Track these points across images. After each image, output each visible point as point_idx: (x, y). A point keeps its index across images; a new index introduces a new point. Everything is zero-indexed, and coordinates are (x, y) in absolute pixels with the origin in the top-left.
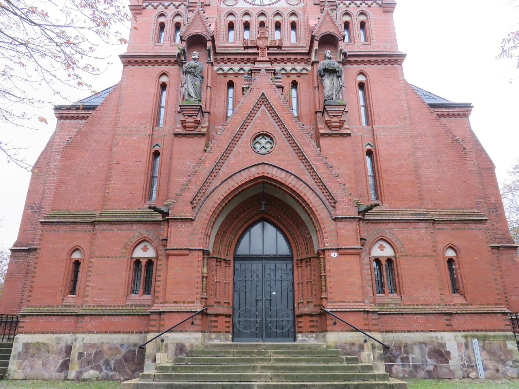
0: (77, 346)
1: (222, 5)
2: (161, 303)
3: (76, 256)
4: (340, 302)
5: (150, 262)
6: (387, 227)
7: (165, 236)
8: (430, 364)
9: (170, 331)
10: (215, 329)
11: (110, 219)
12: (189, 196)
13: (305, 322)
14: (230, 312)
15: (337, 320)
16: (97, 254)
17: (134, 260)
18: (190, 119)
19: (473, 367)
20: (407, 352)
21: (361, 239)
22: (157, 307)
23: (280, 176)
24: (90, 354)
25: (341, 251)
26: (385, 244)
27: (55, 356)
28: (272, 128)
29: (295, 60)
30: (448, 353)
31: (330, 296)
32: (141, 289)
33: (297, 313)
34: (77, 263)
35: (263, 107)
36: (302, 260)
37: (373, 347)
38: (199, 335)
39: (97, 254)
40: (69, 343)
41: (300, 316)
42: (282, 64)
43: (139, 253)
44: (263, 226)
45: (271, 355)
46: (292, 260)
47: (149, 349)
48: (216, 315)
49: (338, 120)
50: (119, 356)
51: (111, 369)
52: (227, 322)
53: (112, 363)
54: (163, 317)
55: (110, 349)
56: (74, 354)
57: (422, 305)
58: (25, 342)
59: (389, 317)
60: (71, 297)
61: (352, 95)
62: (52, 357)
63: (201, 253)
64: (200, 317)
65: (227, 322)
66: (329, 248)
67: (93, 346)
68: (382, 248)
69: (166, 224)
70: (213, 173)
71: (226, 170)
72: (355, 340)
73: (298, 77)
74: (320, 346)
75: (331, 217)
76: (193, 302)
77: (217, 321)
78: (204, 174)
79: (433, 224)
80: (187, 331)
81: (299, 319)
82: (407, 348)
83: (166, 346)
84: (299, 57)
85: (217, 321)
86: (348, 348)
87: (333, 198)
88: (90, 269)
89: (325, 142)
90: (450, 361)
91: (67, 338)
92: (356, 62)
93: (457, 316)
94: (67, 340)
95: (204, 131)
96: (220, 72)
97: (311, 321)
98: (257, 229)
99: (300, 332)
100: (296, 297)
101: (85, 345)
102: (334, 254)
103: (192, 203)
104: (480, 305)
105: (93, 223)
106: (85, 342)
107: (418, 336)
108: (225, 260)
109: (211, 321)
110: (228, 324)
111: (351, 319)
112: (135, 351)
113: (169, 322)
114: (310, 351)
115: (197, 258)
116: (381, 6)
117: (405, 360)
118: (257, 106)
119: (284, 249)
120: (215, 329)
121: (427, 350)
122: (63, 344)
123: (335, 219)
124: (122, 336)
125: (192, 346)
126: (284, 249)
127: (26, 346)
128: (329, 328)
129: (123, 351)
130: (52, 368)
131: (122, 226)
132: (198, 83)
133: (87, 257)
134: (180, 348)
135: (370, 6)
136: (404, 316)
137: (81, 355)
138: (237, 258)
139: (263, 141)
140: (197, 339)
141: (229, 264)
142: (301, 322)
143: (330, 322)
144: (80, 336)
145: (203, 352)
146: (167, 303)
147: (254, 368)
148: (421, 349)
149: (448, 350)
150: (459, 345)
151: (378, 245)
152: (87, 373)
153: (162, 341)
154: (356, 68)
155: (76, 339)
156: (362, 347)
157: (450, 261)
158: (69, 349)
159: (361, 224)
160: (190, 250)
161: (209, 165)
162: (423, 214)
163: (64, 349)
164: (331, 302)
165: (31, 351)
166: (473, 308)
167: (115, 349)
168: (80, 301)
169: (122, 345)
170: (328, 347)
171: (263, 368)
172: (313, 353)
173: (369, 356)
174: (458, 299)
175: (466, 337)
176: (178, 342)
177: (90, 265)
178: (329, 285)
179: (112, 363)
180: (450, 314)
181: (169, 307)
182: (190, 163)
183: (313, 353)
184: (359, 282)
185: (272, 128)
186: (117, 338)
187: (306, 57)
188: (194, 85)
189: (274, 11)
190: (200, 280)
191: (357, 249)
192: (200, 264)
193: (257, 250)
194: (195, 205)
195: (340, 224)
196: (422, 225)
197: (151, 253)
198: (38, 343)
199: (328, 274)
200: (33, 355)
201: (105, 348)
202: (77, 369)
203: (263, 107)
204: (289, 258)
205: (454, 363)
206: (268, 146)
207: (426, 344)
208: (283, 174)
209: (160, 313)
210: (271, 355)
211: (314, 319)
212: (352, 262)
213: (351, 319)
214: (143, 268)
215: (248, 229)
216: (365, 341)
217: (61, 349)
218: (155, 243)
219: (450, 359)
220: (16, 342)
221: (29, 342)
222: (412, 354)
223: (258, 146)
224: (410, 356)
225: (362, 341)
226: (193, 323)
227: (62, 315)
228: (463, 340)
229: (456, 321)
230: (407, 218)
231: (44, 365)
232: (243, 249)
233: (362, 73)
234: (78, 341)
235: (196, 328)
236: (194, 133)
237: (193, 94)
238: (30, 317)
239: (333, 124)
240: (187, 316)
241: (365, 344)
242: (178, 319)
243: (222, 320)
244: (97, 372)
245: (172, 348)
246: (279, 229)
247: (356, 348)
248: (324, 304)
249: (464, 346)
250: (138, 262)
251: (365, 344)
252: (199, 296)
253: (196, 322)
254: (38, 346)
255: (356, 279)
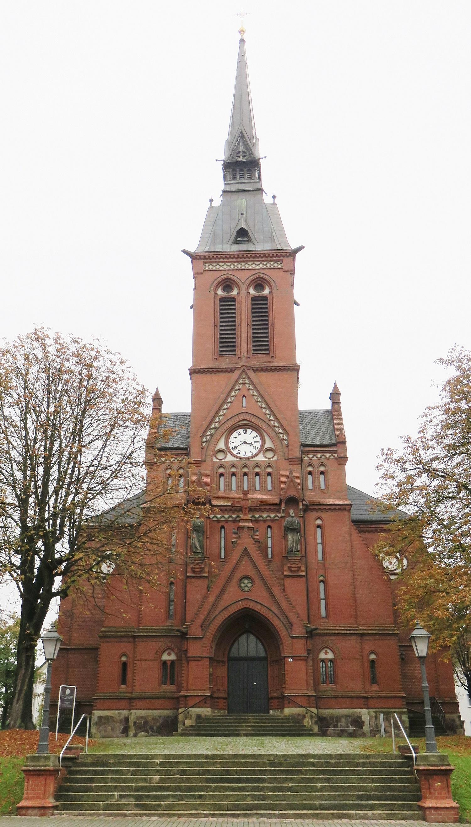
0: (132, 717)
1: (215, 460)
2: (186, 690)
3: (124, 659)
4: (293, 689)
5: (173, 662)
6: (331, 638)
7: (186, 648)
8: (351, 728)
9: (192, 707)
10: (217, 707)
11: (145, 634)
12: (199, 622)
13: (274, 703)
14: (226, 696)
15: (290, 701)
16: (138, 658)
17: (163, 662)
18: (197, 566)
19: (379, 731)
20: (337, 722)
21: (308, 650)
22: (183, 693)
23: (258, 608)
24: (141, 723)
25: (295, 658)
26: (329, 651)
27: (118, 724)
28: (252, 573)
29: (270, 509)
30: (363, 722)
31: (287, 686)
32: (168, 682)
33: (270, 697)
34: (125, 665)
35: (246, 557)
36: (273, 661)
37: (312, 717)
38: (209, 709)
39: (138, 658)
40: (126, 716)
41: (272, 698)
42: (260, 512)
43: (165, 657)
44: (248, 637)
45: (251, 719)
46: (267, 660)
47: (181, 717)
48: (218, 698)
49: (296, 566)
50: (159, 724)
51: (154, 732)
52: (224, 703)
53: (155, 728)
54: (188, 699)
55: (153, 719)
56: (131, 723)
57: (349, 691)
58: (99, 715)
59: (328, 699)
60: (123, 687)
61: (311, 537)
62: (117, 725)
63: (208, 660)
64: (209, 698)
65: (224, 703)
66: (287, 655)
67: (142, 717)
68: (326, 653)
69: (186, 641)
70: (214, 606)
71: (223, 604)
72: (301, 712)
73: (272, 522)
74: (280, 716)
75: (290, 635)
76: (205, 690)
77: (218, 702)
78: (208, 607)
79: (361, 636)
80: (202, 707)
81: (271, 701)
82: (338, 719)
83: (191, 716)
84: (272, 507)
85: (218, 702)
86: (296, 717)
87: (290, 623)
88: (135, 668)
89: (288, 582)
90: (364, 727)
91: (125, 713)
92: (315, 509)
93: (372, 699)
94: (125, 714)
95: (207, 575)
96: (215, 519)
97: (278, 702)
98: (243, 638)
99: (271, 710)
100: (269, 686)
101: (137, 717)
102: (290, 660)
103: (201, 626)
104: (387, 691)
105: (134, 637)
106: (137, 715)
107: (345, 712)
108: (222, 661)
109: (215, 702)
110: (225, 704)
111: (298, 700)
112: (168, 720)
113: (191, 702)
114: (274, 718)
115: (206, 662)
116: (336, 459)
117: (336, 726)
118: (242, 556)
119: (262, 653)
120: (217, 707)
121: (350, 720)
122: (122, 717)
123: (292, 637)
124: (159, 711)
125: (206, 715)
126: (262, 653)
127: (100, 718)
128: (286, 706)
129: (161, 721)
130: (118, 732)
131: (154, 639)
132: (201, 538)
133: (131, 660)
134: (199, 717)
135: (328, 459)
136: (337, 699)
137: (135, 723)
138: (230, 659)
139: (246, 581)
140: (208, 712)
141: (225, 663)
142: (272, 703)
143: (286, 702)
144: (133, 712)
145: (212, 719)
146: (189, 690)
147: (242, 726)
148: (347, 720)
149: (363, 720)
150: (370, 717)
151: (324, 651)
152: (140, 734)
153: (188, 713)
154: (314, 514)
155: (131, 713)
156: (304, 717)
157: (373, 661)
158: (127, 719)
159: (308, 641)
160: (201, 657)
161: (211, 599)
162: (355, 630)
163: (123, 720)
164: (288, 690)
165: (103, 721)
166: (383, 694)
167: (155, 719)
168: (129, 690)
169: (160, 717)
170: (284, 716)
171: (246, 726)
172: (276, 719)
173: (308, 722)
174: (375, 688)
175: (376, 712)
176: (197, 713)
177: (135, 665)
178: (287, 679)
179: (155, 728)
180: (367, 698)
181: (191, 693)
182: (199, 597)
183: (276, 719)
184: (305, 677)
185: (252, 573)
186: (156, 713)
187: (278, 507)
188: (199, 540)
189: (253, 464)
190: (208, 676)
191: (304, 656)
192: (208, 666)
193: (243, 653)
194: (203, 628)
195: (295, 640)
196: (353, 637)
197: (173, 657)
198: (107, 716)
199: (286, 673)
200: (105, 724)
201: (150, 718)
202: (134, 732)
203: (246, 557)
204: (265, 659)
205: (366, 728)
206: (250, 585)
207: (349, 716)
208: (259, 607)
209: (186, 697)
210: (251, 719)
211: (279, 700)
212: (301, 665)
213: (298, 700)
214: (169, 667)
215: (237, 639)
216: (307, 713)
217: (122, 720)
218: (176, 651)
219: (364, 726)
220: (93, 715)
221: (102, 715)
222: (340, 722)
223: (243, 585)
224: (339, 724)
225: (305, 713)
226: (205, 702)
227: (120, 699)
228: (373, 714)
229: (371, 702)
230: (343, 632)
231: (113, 729)
232: (234, 653)
233: (319, 518)
234: (132, 715)
235: (207, 705)
236: (200, 575)
237: (198, 547)
238: (100, 700)
239: (293, 569)
240: (202, 698)
241: (306, 715)
242: (196, 700)
243: (221, 701)
244: (146, 734)
245: (194, 717)
246: (258, 638)
247: (301, 717)
248: (284, 691)
249: (374, 718)
250: (165, 662)
251: (306, 715)
252: (208, 686)
253: (208, 702)
254: (107, 718)
255: (303, 676)
